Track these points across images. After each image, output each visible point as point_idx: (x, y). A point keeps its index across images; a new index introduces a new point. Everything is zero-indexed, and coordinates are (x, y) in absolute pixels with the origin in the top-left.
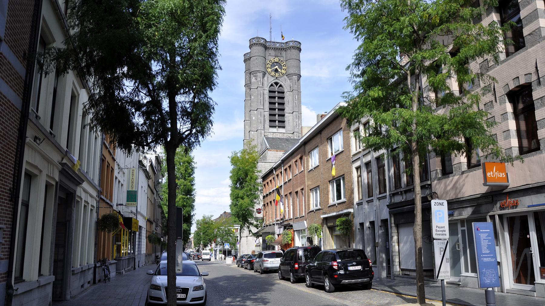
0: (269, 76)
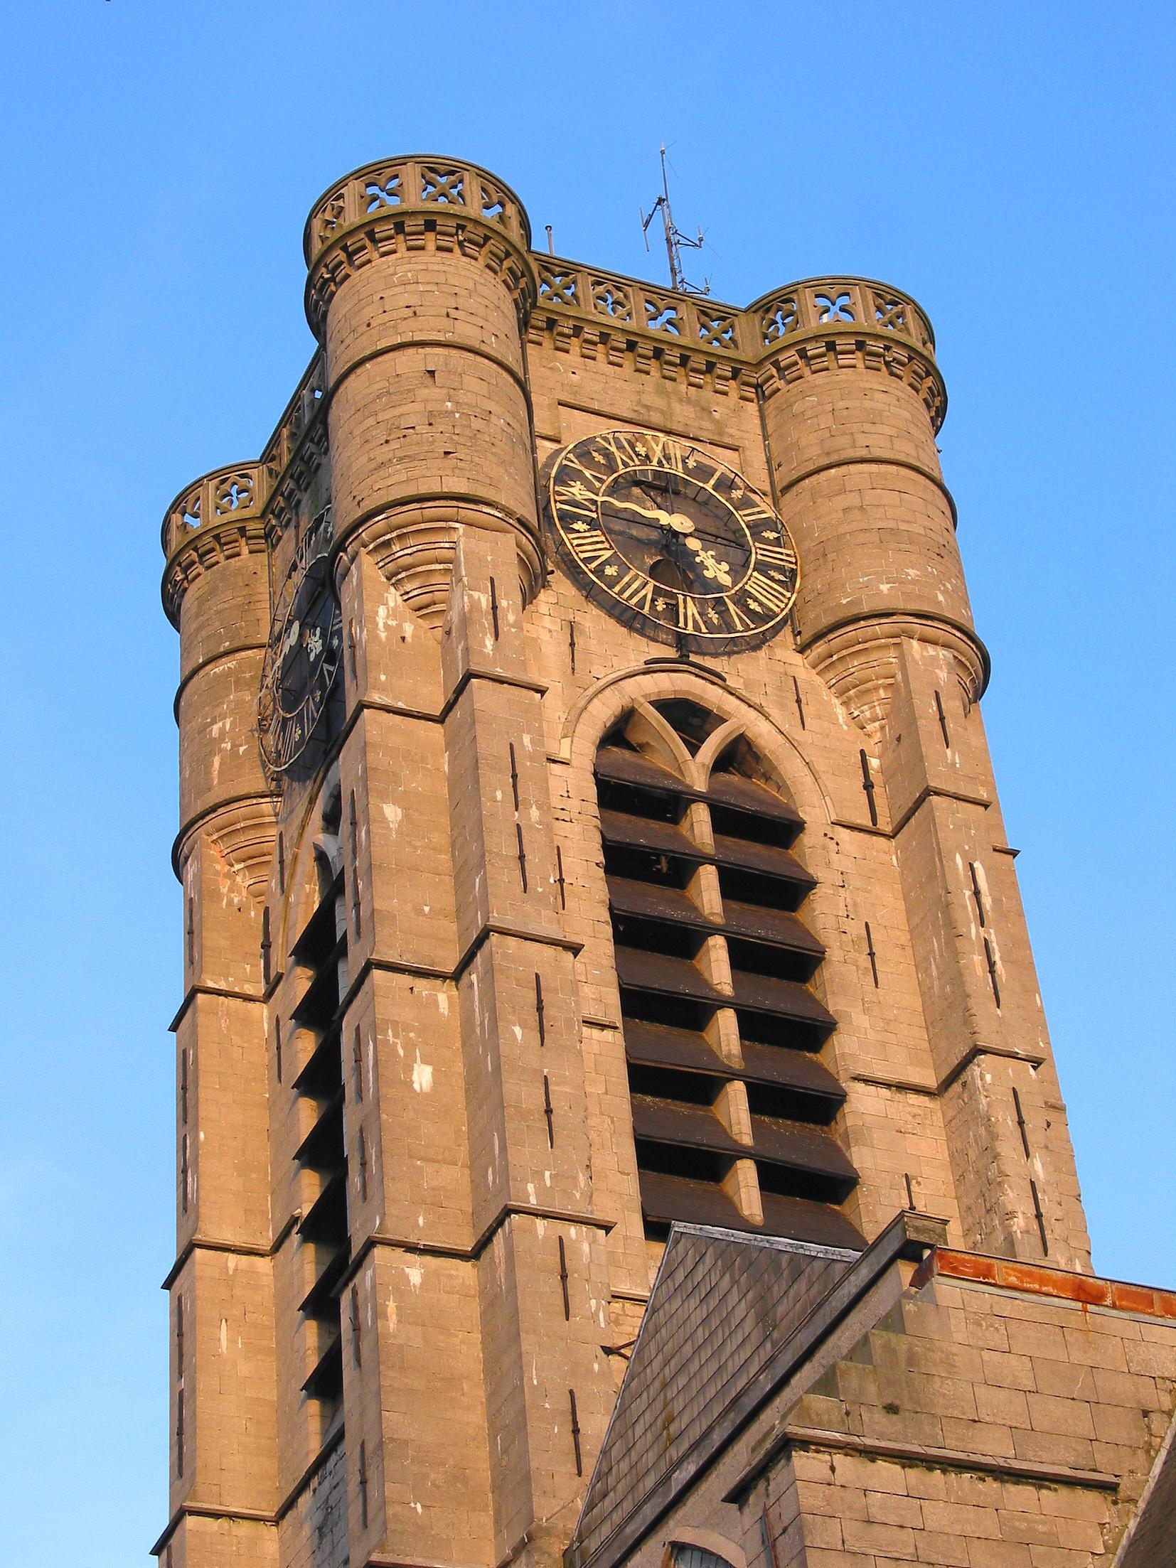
0: (593, 620)
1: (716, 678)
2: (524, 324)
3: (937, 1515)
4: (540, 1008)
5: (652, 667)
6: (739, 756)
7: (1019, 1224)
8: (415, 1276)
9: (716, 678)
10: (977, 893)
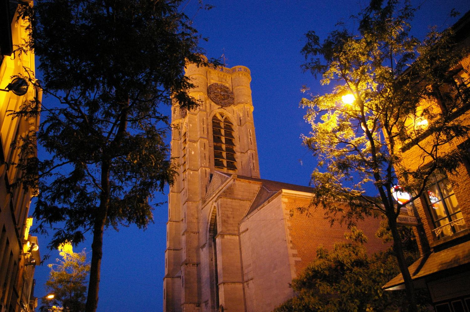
3: (233, 203)
4: (205, 146)
7: (252, 167)
8: (191, 173)
10: (250, 133)
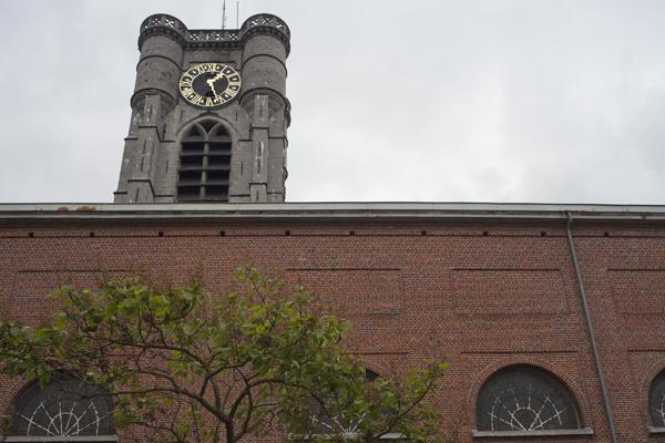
1: (216, 115)
2: (184, 48)
5: (201, 115)
6: (223, 131)
9: (216, 115)
